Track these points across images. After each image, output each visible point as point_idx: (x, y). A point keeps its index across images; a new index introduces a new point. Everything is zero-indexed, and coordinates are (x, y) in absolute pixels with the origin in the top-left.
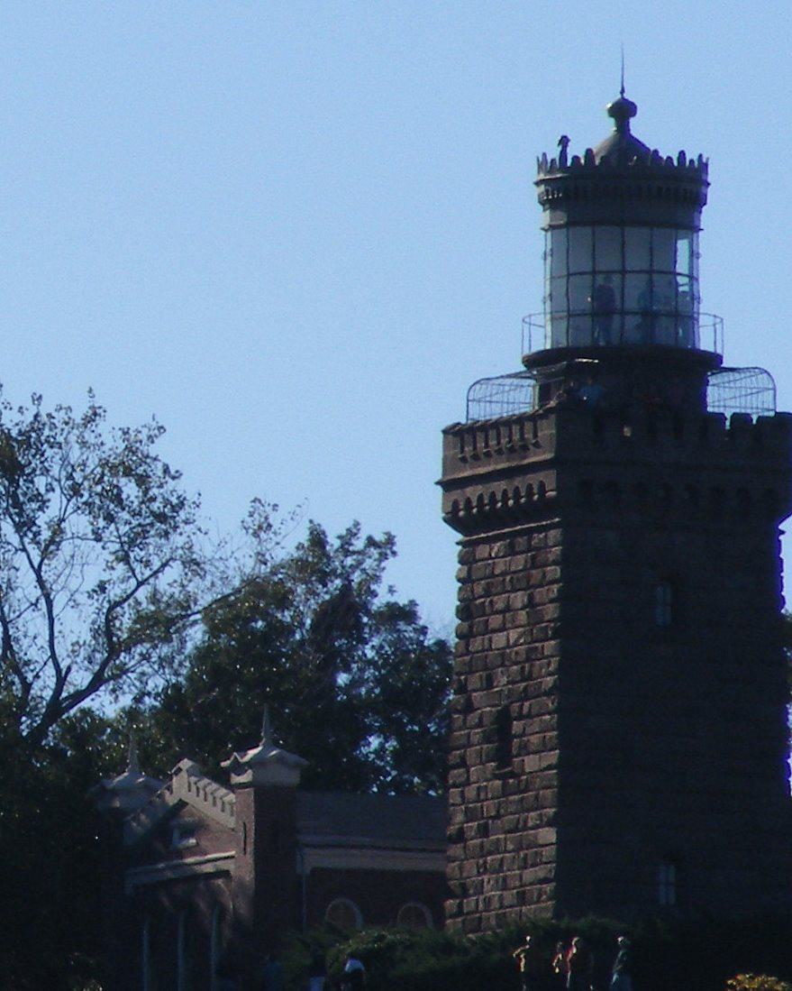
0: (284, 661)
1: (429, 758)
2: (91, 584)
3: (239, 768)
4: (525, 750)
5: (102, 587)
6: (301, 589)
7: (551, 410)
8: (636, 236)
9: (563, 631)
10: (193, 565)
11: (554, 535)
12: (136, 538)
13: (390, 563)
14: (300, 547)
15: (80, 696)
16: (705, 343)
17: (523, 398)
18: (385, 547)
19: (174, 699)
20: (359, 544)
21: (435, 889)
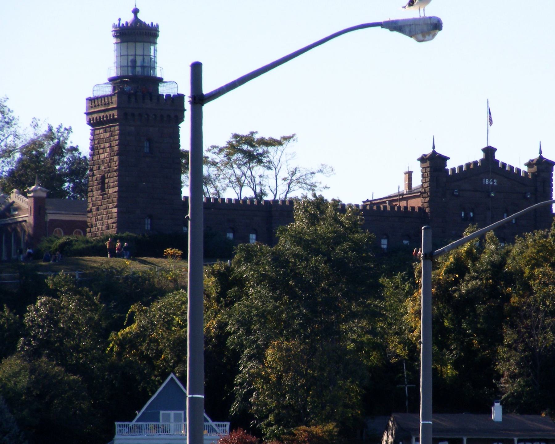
3: (29, 192)
4: (109, 187)
8: (139, 45)
10: (16, 136)
11: (117, 128)
16: (158, 75)
18: (69, 130)
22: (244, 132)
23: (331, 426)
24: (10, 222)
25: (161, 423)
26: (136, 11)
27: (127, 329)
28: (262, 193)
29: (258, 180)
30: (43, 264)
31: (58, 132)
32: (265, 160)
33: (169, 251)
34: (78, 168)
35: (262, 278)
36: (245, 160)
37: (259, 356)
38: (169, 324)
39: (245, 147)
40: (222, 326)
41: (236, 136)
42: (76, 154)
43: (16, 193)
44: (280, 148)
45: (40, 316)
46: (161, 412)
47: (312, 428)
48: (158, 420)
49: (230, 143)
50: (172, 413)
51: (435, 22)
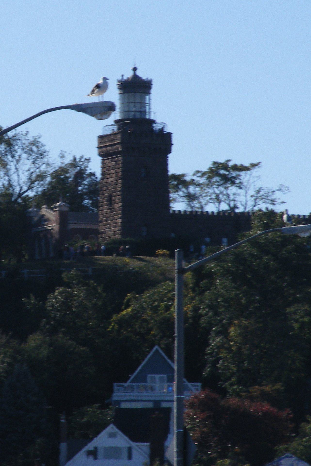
0: (66, 186)
1: (96, 204)
2: (27, 169)
3: (56, 207)
4: (115, 203)
5: (29, 170)
6: (71, 169)
7: (120, 132)
8: (138, 95)
9: (123, 178)
10: (48, 164)
11: (121, 158)
12: (36, 159)
13: (90, 164)
14: (71, 161)
15: (25, 192)
16: (152, 118)
17: (115, 128)
18: (88, 160)
19: (44, 193)
20: (83, 160)
21: (96, 232)
22: (222, 160)
23: (278, 386)
24: (42, 229)
25: (149, 384)
26: (135, 69)
27: (124, 312)
28: (235, 207)
29: (232, 197)
30: (66, 262)
31: (80, 161)
32: (237, 181)
33: (160, 251)
34: (94, 190)
35: (227, 272)
36: (222, 182)
37: (224, 332)
38: (155, 309)
39: (222, 172)
40: (196, 309)
41: (215, 163)
42: (93, 177)
43: (46, 208)
44: (248, 172)
45: (57, 302)
46: (149, 376)
47: (263, 388)
48: (146, 382)
49: (210, 168)
50: (157, 376)
51: (110, 105)
